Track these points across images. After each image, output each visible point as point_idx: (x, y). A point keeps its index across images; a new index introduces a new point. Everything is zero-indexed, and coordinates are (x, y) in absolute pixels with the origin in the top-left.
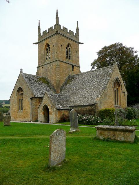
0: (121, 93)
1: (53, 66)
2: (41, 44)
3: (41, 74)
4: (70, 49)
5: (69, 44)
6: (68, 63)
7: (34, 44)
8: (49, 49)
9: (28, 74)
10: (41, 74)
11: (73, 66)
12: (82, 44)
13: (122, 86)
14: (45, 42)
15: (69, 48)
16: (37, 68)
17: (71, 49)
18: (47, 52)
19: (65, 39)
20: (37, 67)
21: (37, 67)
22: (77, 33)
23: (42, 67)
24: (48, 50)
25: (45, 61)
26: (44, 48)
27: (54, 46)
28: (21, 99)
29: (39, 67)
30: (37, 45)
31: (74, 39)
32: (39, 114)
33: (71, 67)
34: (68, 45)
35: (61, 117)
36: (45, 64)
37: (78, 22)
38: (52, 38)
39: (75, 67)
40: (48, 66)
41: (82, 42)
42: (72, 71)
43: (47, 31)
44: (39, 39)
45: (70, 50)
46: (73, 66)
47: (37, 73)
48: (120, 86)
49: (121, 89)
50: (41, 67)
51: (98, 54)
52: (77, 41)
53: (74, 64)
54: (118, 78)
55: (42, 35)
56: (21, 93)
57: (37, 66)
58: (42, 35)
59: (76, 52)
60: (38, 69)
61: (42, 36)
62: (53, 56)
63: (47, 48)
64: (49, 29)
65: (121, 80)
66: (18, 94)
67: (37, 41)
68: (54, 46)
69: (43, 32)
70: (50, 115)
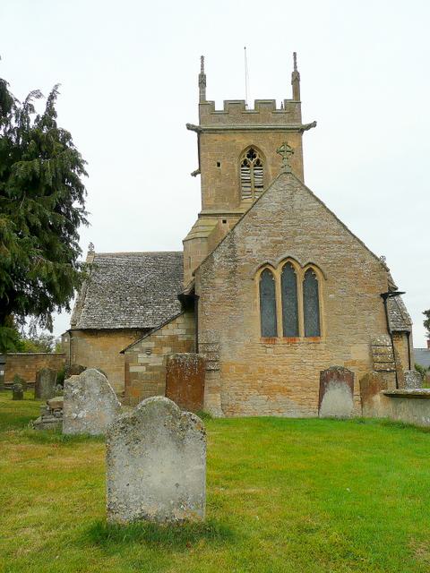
22: (294, 105)
45: (249, 166)
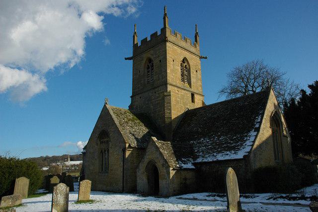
6: (185, 88)
7: (126, 59)
8: (152, 66)
11: (193, 95)
13: (136, 201)
14: (146, 56)
18: (148, 72)
19: (179, 50)
24: (150, 68)
27: (160, 61)
28: (105, 151)
29: (135, 95)
30: (132, 60)
32: (138, 179)
33: (190, 95)
34: (183, 60)
35: (181, 183)
37: (206, 58)
39: (195, 96)
42: (191, 101)
43: (149, 39)
44: (134, 52)
46: (192, 94)
50: (137, 97)
51: (236, 69)
56: (105, 140)
57: (131, 95)
59: (197, 71)
63: (148, 66)
64: (152, 36)
67: (131, 55)
70: (160, 181)
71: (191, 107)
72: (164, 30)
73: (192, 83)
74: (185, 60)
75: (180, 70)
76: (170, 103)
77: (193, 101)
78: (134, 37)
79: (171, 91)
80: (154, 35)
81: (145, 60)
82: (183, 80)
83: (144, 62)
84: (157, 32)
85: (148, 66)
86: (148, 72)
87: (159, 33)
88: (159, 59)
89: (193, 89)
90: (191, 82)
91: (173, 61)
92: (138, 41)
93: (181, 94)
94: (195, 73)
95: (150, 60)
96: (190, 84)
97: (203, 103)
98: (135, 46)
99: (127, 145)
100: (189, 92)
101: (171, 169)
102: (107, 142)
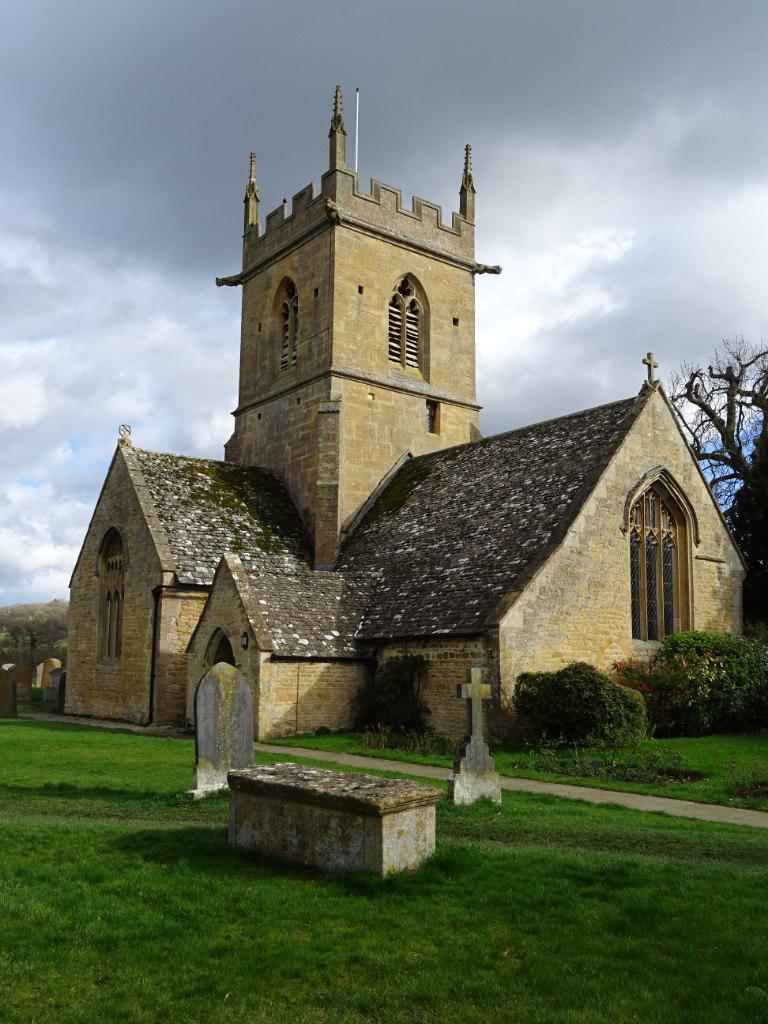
0: (693, 559)
1: (307, 405)
2: (257, 281)
3: (249, 451)
4: (413, 303)
5: (410, 274)
9: (605, 403)
10: (249, 451)
11: (433, 404)
12: (496, 271)
14: (276, 272)
15: (410, 299)
16: (233, 418)
17: (420, 306)
20: (234, 414)
21: (234, 414)
23: (260, 409)
25: (274, 376)
26: (270, 303)
27: (316, 291)
28: (117, 593)
30: (240, 287)
31: (444, 244)
34: (405, 283)
36: (272, 393)
38: (308, 247)
39: (443, 408)
40: (284, 403)
41: (491, 264)
43: (288, 212)
46: (429, 403)
47: (232, 446)
48: (683, 523)
49: (691, 537)
50: (252, 415)
52: (460, 255)
53: (441, 393)
54: (665, 472)
55: (261, 231)
57: (235, 405)
58: (261, 231)
59: (456, 321)
60: (237, 424)
61: (265, 237)
62: (310, 349)
63: (285, 306)
64: (297, 198)
65: (24, 538)
66: (101, 567)
67: (237, 270)
68: (316, 291)
69: (269, 218)
71: (422, 445)
72: (329, 178)
73: (433, 364)
74: (408, 283)
75: (386, 321)
76: (333, 438)
77: (433, 425)
78: (247, 201)
79: (344, 396)
80: (302, 198)
81: (275, 285)
82: (396, 354)
83: (272, 292)
84: (311, 186)
85: (285, 306)
86: (286, 328)
87: (317, 192)
88: (314, 287)
89: (435, 390)
90: (428, 361)
91: (361, 290)
92: (259, 217)
93: (384, 406)
94: (448, 326)
95: (289, 287)
96: (425, 368)
97: (475, 432)
98: (250, 230)
99: (168, 579)
100: (416, 399)
101: (264, 656)
102: (120, 568)
